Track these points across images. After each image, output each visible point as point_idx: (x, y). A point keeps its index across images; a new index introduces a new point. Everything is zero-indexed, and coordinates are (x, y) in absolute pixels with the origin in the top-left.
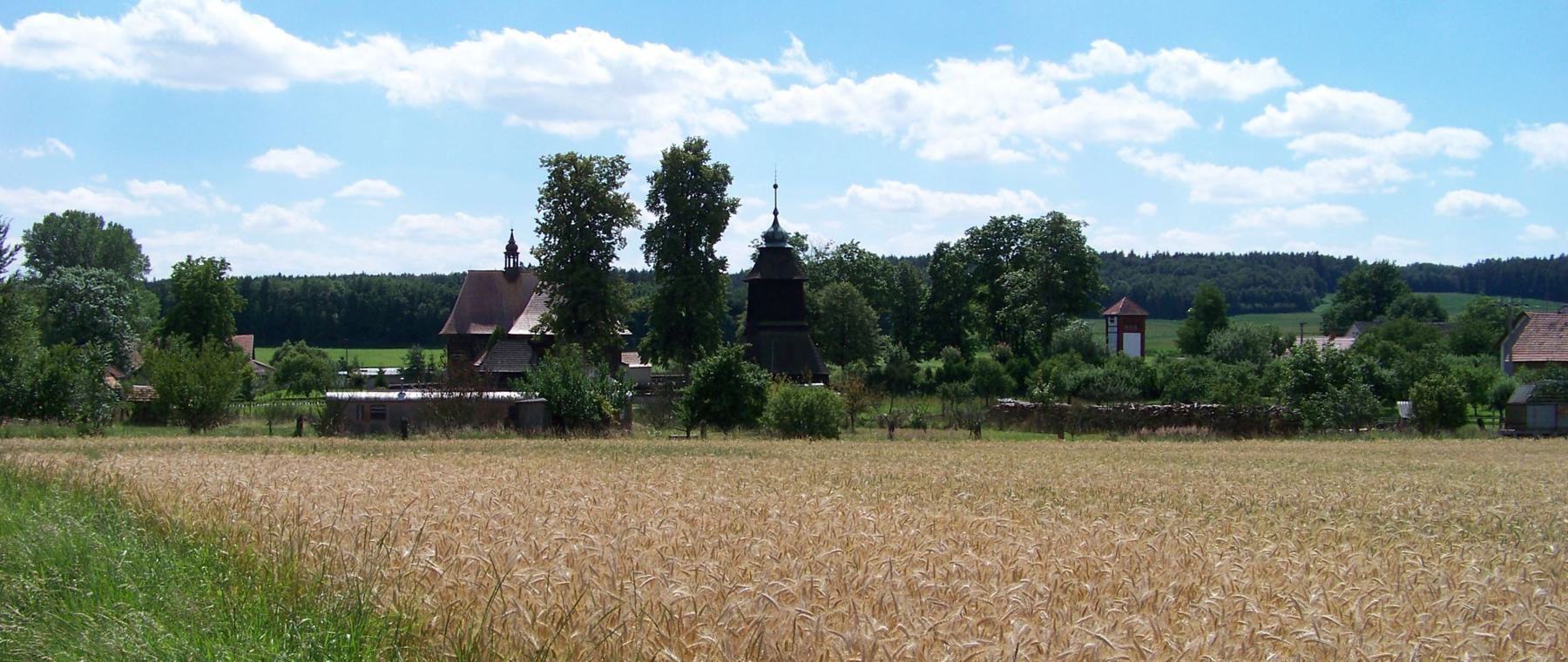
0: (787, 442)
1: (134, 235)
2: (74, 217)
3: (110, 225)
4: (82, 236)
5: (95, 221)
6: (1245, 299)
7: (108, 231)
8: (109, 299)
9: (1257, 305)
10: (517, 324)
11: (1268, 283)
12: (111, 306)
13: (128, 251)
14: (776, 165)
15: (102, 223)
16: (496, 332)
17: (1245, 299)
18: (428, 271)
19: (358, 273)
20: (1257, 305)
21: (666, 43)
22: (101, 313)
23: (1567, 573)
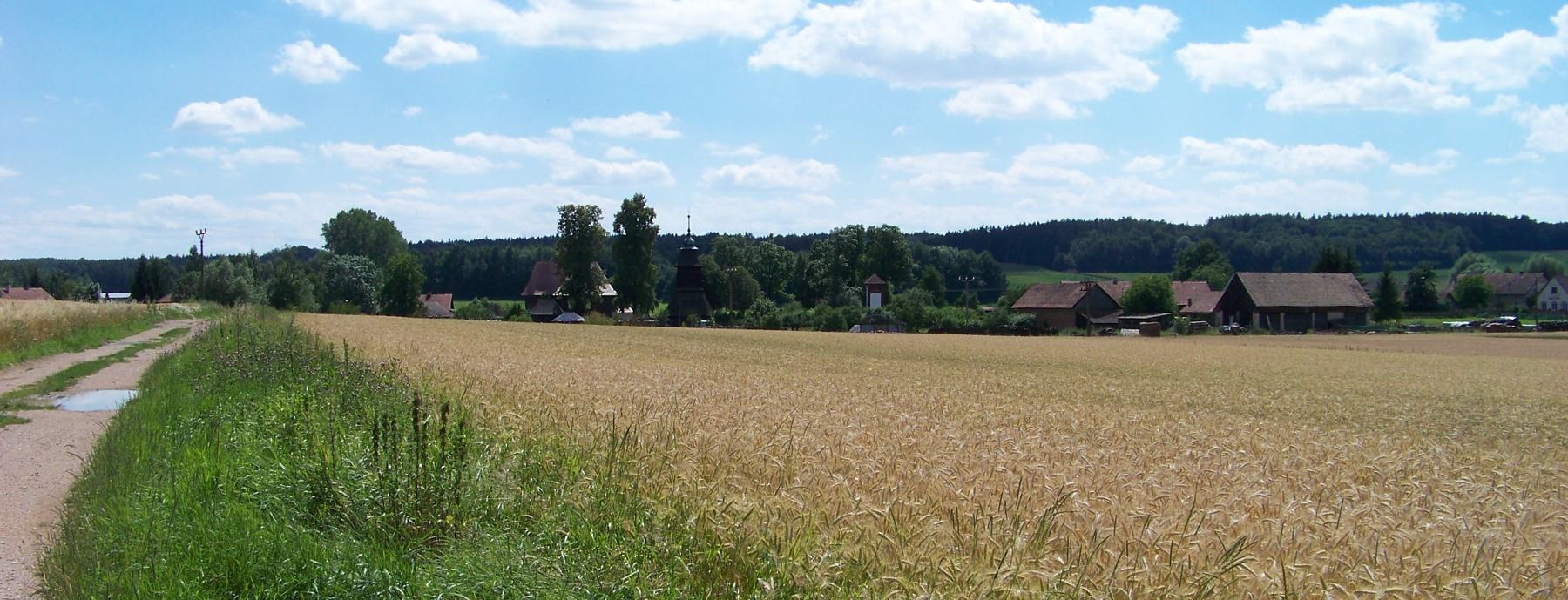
0: (77, 354)
1: (395, 225)
2: (356, 213)
3: (380, 218)
4: (361, 227)
5: (371, 215)
6: (1390, 257)
7: (378, 223)
8: (364, 274)
9: (1401, 263)
10: (1244, 274)
11: (1415, 243)
12: (364, 278)
13: (390, 236)
14: (201, 234)
15: (376, 217)
16: (543, 295)
17: (1390, 257)
18: (1155, 217)
19: (935, 233)
20: (1401, 263)
21: (1290, 16)
22: (358, 282)
23: (1566, 491)
